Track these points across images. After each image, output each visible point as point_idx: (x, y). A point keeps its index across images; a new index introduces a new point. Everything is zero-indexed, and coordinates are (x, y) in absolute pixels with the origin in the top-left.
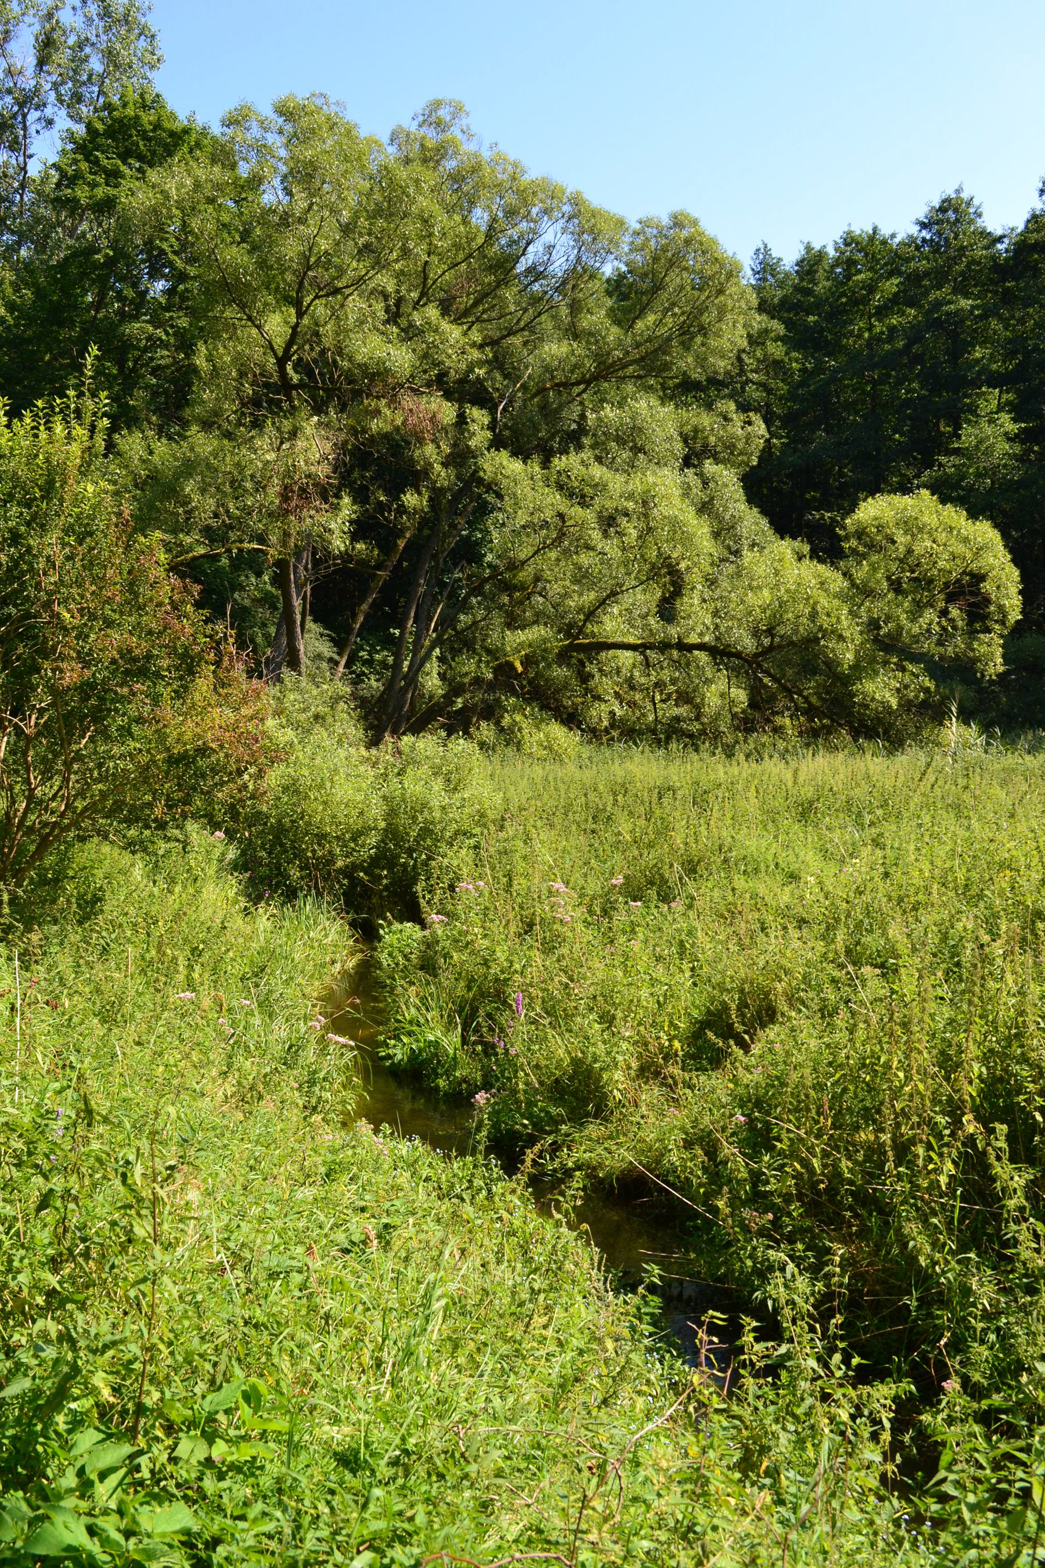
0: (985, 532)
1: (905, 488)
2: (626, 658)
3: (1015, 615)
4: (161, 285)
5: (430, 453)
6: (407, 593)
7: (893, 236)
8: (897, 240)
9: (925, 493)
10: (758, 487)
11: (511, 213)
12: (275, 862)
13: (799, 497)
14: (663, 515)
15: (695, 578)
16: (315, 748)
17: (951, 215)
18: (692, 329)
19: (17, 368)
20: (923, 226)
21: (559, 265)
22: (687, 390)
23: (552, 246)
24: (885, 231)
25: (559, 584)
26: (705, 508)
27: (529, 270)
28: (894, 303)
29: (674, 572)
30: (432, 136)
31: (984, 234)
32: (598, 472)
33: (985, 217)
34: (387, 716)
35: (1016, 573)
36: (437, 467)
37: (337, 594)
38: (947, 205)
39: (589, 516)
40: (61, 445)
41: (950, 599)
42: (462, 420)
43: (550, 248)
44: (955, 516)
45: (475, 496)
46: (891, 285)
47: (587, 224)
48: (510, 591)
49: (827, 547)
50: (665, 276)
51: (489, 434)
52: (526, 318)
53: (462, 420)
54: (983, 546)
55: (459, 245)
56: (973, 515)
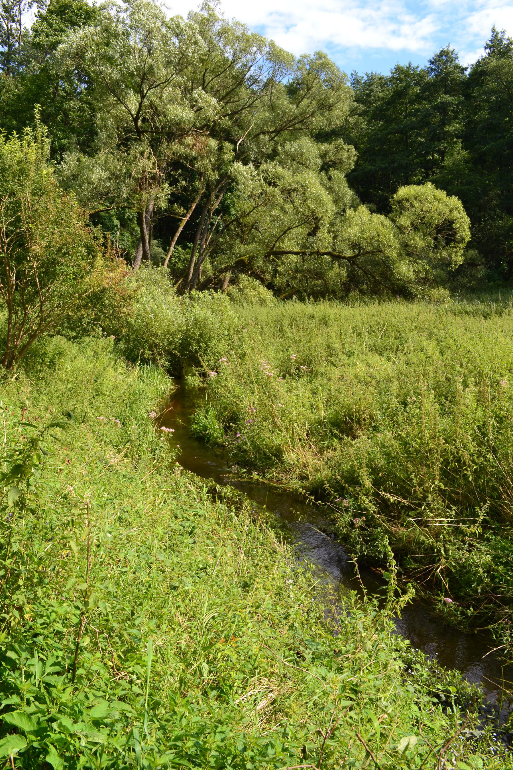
0: (455, 201)
1: (419, 183)
2: (294, 258)
3: (468, 238)
4: (84, 86)
5: (205, 164)
6: (191, 224)
7: (418, 67)
8: (419, 69)
9: (429, 184)
10: (352, 180)
11: (243, 51)
12: (134, 350)
13: (373, 187)
14: (307, 190)
15: (326, 221)
16: (154, 299)
17: (444, 58)
18: (325, 106)
19: (13, 118)
20: (432, 63)
21: (264, 78)
22: (321, 137)
23: (260, 68)
24: (414, 65)
25: (267, 228)
26: (330, 190)
27: (250, 78)
28: (418, 98)
29: (317, 219)
30: (205, 14)
31: (457, 67)
32: (280, 169)
33: (459, 59)
34: (184, 280)
35: (468, 220)
36: (210, 171)
37: (164, 227)
38: (442, 53)
39: (277, 190)
40: (26, 149)
41: (438, 232)
42: (221, 149)
43: (260, 68)
44: (442, 194)
45: (228, 183)
46: (417, 90)
47: (276, 57)
48: (244, 229)
49: (383, 207)
50: (311, 80)
51: (233, 153)
52: (251, 101)
53: (221, 149)
54: (450, 206)
55: (213, 63)
56: (449, 194)
